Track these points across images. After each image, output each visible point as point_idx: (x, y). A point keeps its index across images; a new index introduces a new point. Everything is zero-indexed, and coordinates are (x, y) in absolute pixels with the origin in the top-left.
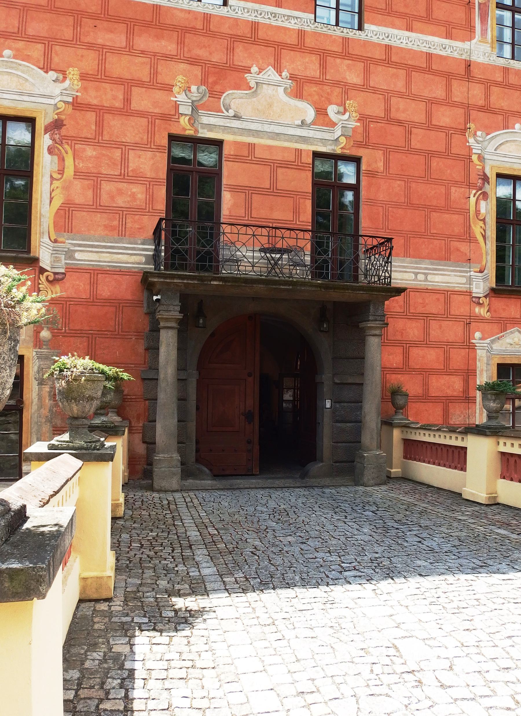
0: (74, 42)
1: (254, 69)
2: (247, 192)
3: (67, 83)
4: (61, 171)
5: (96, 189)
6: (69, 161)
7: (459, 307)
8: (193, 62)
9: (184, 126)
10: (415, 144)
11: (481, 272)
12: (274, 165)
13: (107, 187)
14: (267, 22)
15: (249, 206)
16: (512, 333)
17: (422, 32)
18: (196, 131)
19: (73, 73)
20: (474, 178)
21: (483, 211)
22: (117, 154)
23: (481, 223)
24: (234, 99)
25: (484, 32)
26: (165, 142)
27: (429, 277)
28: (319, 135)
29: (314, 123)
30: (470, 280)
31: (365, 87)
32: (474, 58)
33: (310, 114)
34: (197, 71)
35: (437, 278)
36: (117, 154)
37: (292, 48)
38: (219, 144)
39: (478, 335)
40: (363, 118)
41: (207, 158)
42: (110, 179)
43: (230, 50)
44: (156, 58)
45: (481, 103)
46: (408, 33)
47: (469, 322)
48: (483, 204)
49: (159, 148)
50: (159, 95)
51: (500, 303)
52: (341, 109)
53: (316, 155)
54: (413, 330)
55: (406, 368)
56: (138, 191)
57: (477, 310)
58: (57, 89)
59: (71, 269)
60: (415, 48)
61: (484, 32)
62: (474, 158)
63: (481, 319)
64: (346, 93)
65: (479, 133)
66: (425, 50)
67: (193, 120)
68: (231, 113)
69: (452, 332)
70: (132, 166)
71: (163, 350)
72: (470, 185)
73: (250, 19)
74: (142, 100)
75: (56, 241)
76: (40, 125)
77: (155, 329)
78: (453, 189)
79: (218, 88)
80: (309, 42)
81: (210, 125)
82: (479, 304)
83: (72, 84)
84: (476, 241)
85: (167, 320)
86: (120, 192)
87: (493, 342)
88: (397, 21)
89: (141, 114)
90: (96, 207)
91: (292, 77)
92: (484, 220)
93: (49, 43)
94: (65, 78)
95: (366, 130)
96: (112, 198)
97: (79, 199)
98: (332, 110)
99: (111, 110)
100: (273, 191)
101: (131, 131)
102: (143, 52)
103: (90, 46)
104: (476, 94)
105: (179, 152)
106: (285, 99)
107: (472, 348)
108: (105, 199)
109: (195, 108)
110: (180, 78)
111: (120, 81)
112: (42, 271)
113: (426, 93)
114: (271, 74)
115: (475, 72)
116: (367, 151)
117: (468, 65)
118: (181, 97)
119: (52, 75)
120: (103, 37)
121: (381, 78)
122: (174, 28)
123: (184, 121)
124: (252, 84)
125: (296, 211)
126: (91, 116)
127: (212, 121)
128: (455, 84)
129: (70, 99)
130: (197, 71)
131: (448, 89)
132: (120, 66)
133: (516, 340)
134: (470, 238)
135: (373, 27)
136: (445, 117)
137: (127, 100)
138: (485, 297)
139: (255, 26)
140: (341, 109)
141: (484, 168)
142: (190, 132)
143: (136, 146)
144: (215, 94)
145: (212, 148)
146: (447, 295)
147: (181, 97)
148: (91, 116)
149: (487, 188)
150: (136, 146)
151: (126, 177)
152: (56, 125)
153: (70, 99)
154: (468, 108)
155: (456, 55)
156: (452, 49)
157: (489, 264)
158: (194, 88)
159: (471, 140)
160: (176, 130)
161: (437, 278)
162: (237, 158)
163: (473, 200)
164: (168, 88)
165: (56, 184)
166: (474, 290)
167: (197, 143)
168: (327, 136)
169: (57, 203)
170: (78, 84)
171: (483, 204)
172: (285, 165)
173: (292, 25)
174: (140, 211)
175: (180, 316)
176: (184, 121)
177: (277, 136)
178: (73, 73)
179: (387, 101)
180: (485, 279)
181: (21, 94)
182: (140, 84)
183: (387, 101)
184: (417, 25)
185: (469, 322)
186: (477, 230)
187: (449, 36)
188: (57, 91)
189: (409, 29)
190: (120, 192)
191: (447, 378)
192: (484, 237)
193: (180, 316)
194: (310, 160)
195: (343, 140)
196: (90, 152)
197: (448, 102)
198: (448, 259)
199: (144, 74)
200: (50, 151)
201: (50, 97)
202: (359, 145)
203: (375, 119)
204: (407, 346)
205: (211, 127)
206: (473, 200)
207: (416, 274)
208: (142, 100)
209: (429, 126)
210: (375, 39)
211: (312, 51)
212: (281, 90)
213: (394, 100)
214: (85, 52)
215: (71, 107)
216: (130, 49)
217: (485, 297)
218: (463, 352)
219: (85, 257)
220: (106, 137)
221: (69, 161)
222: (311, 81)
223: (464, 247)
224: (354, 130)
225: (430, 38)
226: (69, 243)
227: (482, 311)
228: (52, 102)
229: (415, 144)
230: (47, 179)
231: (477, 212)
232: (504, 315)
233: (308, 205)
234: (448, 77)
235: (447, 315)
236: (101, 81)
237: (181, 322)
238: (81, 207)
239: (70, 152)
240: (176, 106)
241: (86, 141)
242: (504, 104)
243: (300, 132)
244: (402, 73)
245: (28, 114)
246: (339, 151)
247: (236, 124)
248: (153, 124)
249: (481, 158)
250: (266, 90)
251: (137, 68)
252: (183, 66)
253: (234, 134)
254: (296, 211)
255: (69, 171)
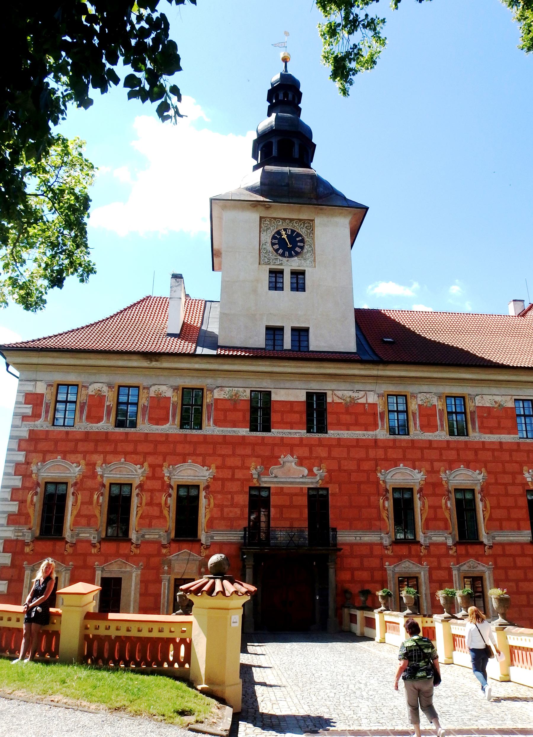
0: (214, 454)
1: (282, 456)
2: (281, 508)
3: (211, 471)
4: (209, 505)
5: (222, 511)
6: (212, 500)
7: (377, 551)
8: (258, 457)
9: (255, 483)
10: (353, 479)
11: (387, 534)
12: (291, 495)
13: (226, 510)
14: (287, 436)
15: (281, 513)
16: (405, 562)
17: (354, 430)
18: (260, 484)
19: (213, 466)
20: (381, 491)
21: (387, 505)
22: (230, 496)
23: (386, 511)
24: (275, 470)
25: (383, 425)
26: (248, 490)
27: (362, 538)
28: (310, 480)
29: (307, 475)
30: (381, 538)
31: (330, 457)
32: (378, 437)
33: (306, 472)
34: (260, 460)
35: (366, 538)
36: (230, 496)
37: (297, 445)
38: (269, 488)
39: (387, 563)
40: (329, 471)
41: (264, 494)
42: (227, 506)
43: (273, 450)
44: (243, 456)
45: (383, 457)
46: (347, 432)
47: (382, 558)
48: (386, 503)
49: (245, 492)
50: (245, 471)
51: (397, 548)
52: (319, 468)
53: (309, 489)
54: (355, 563)
55: (352, 580)
56: (238, 511)
57: (386, 552)
58: (207, 473)
59: (213, 543)
60: (351, 437)
61: (383, 425)
62: (381, 482)
63: (388, 556)
64: (321, 461)
65: (383, 471)
66: (355, 437)
67: (258, 479)
68: (273, 475)
69: (375, 563)
70: (235, 501)
71: (429, 373)
72: (379, 495)
73: (280, 436)
74: (239, 474)
75: (207, 533)
76: (201, 488)
77: (244, 567)
78: (372, 497)
79: (268, 466)
80: (305, 442)
81: (266, 481)
82: (387, 549)
83: (213, 470)
84: (384, 520)
85: (248, 565)
86: (231, 512)
87: (395, 566)
88: (342, 427)
89: (238, 480)
90: (222, 518)
91: (298, 458)
92: (387, 510)
93: (204, 456)
94: (210, 469)
95: (330, 475)
96: (228, 514)
97: (215, 516)
98: (315, 469)
99: (227, 479)
100: (291, 506)
101: (234, 487)
102: (239, 455)
103: (219, 455)
104: (380, 453)
105: (253, 493)
106: (295, 467)
107: (385, 570)
108: (225, 515)
109: (259, 475)
110: (253, 464)
111: (230, 468)
112: (202, 544)
113: (357, 456)
114: (289, 458)
115: (380, 444)
116: (331, 485)
117: (376, 441)
118: (254, 471)
119: (206, 468)
120: (223, 452)
121: (336, 453)
122: (250, 444)
123: (255, 481)
124: (282, 462)
125: (301, 513)
126: (220, 483)
127: (266, 479)
128: (370, 450)
129: (212, 477)
130: (260, 460)
131: (367, 453)
132: (230, 462)
133: (407, 565)
134: (380, 518)
135: (332, 432)
136: (366, 466)
137: (233, 475)
138: (390, 545)
139: (282, 439)
140: (319, 468)
141: (386, 486)
142: (257, 485)
143: (237, 493)
144: (267, 469)
145: (266, 490)
146: (371, 545)
147: (254, 471)
148: (220, 483)
149: (388, 495)
150: (237, 493)
151: (233, 505)
152: (207, 488)
153: (212, 477)
154: (376, 460)
155: (370, 437)
156: (369, 435)
157: (391, 530)
158: (258, 467)
159: (379, 474)
160: (252, 485)
161: (366, 538)
162: (276, 494)
163: (381, 501)
164: (249, 468)
165: (207, 510)
166: (384, 543)
167: (260, 489)
168: (313, 480)
169: (207, 517)
170: (215, 471)
171: (386, 503)
172: (296, 495)
173: (297, 436)
174: (239, 519)
175: (253, 564)
176: (255, 481)
177: (291, 483)
178: (213, 466)
179: (339, 462)
180: (389, 537)
181: (195, 476)
182: (238, 468)
183: (339, 462)
184: (351, 427)
185: (382, 558)
186: (384, 515)
187: (366, 430)
188: (208, 474)
189: (348, 430)
190: (231, 512)
191: (373, 584)
192: (388, 518)
193: (253, 564)
194: (306, 491)
195: (320, 481)
196: (219, 496)
197: (367, 459)
198: (371, 529)
199: (239, 464)
200: (205, 497)
201: (205, 476)
202: (327, 483)
203: (334, 471)
204: (353, 570)
205: (265, 482)
206: (381, 501)
207: (356, 537)
208: (239, 474)
209: (359, 470)
210: (333, 437)
211: (306, 446)
212: (293, 464)
213: (342, 462)
214: (217, 458)
215: (212, 480)
216: (234, 455)
217: (390, 545)
218: (380, 572)
219: (217, 538)
220: (226, 490)
221: (212, 500)
222: (306, 458)
223: (378, 523)
224: (325, 476)
225: (357, 432)
226: (212, 533)
227: (389, 553)
228: (206, 478)
229: (353, 479)
230: (204, 509)
231: (384, 506)
232: (400, 553)
233: (306, 510)
234: (367, 447)
235: (371, 555)
236: (222, 468)
237: (254, 566)
238: (216, 519)
239: (212, 497)
240: (252, 475)
241: (218, 492)
242: (394, 456)
243: (301, 480)
244: (345, 449)
245: (202, 387)
246: (319, 486)
247: (275, 480)
248: (243, 483)
249: (384, 482)
250: (288, 464)
251: (237, 462)
252: (254, 459)
253: (274, 484)
254: (301, 513)
255: (212, 505)
